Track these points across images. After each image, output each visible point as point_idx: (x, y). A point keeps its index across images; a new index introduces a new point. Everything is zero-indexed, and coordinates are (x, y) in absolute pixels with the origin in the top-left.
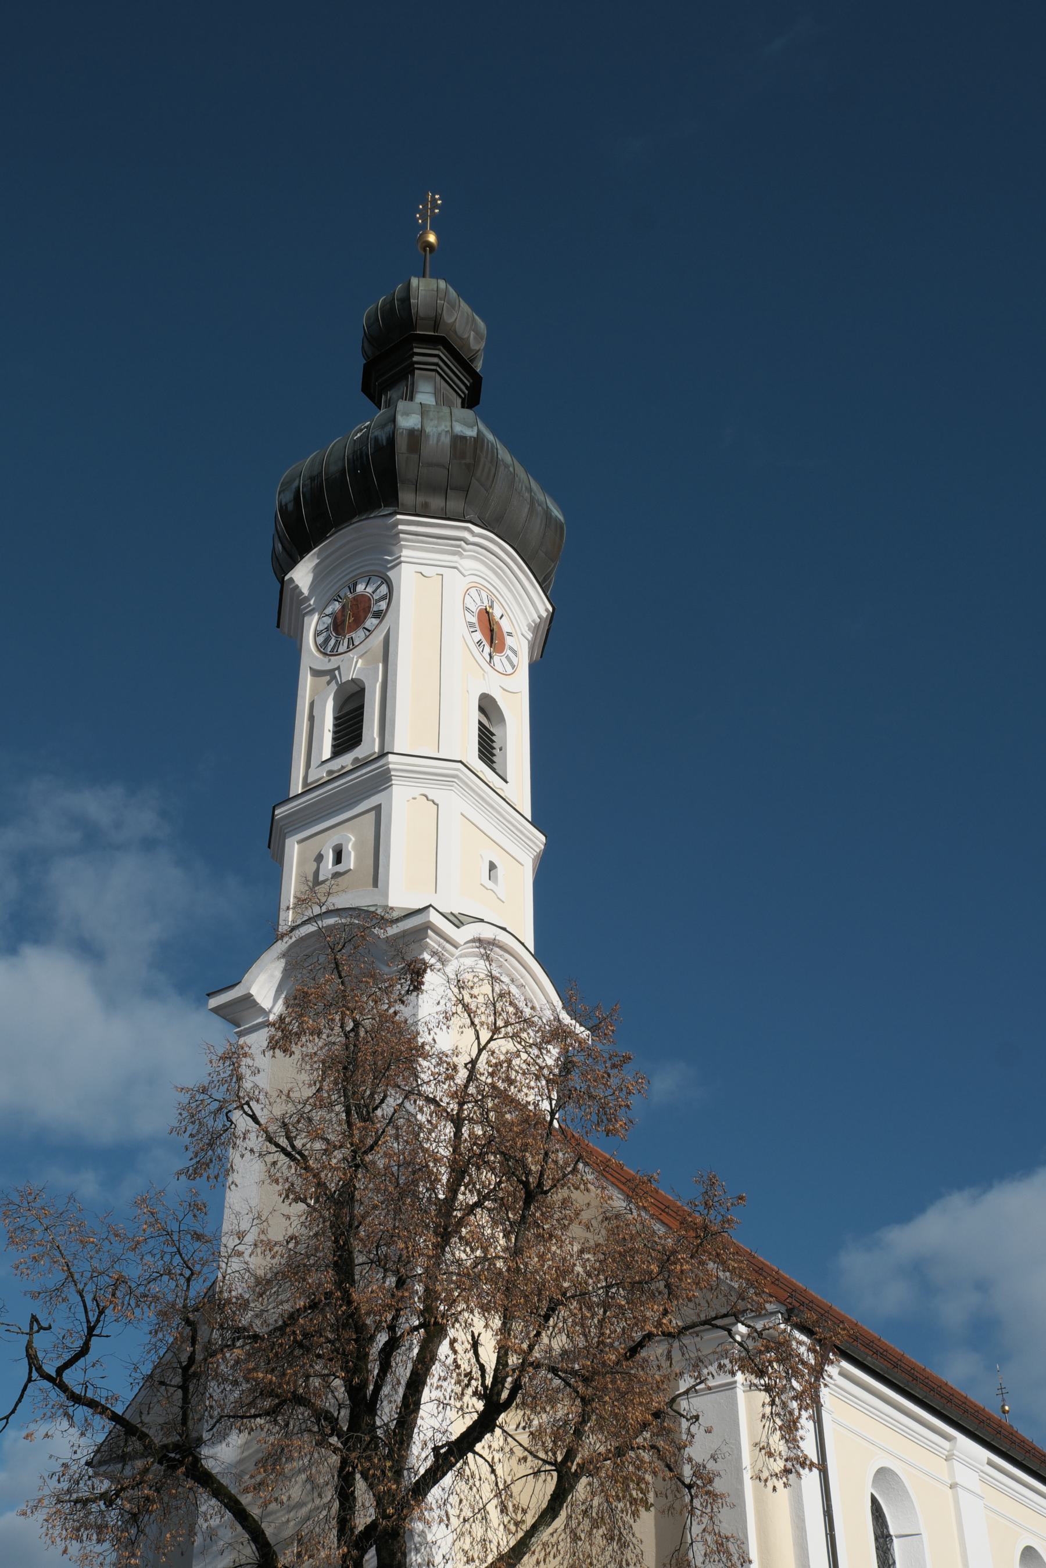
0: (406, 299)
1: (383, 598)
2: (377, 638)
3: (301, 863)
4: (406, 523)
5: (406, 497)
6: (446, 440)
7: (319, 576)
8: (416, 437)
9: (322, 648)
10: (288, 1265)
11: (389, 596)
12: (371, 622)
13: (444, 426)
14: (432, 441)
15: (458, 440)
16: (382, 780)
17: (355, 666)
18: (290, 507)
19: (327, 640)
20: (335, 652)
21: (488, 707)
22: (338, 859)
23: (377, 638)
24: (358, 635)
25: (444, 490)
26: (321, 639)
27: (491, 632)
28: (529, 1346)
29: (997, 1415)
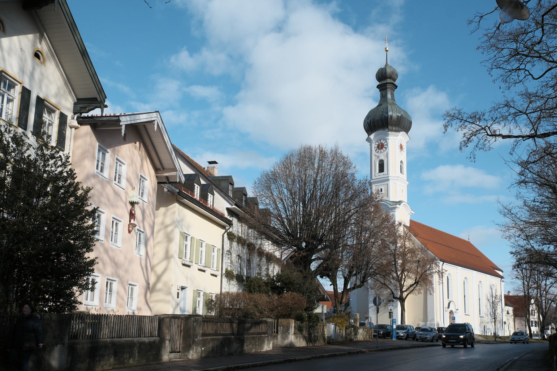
0: (386, 73)
2: (385, 153)
4: (390, 133)
5: (390, 127)
7: (375, 136)
8: (391, 116)
10: (547, 254)
11: (387, 145)
12: (384, 149)
15: (398, 117)
16: (388, 180)
17: (382, 157)
20: (378, 152)
21: (401, 162)
22: (381, 191)
24: (382, 151)
25: (395, 126)
27: (401, 147)
28: (367, 281)
29: (468, 240)
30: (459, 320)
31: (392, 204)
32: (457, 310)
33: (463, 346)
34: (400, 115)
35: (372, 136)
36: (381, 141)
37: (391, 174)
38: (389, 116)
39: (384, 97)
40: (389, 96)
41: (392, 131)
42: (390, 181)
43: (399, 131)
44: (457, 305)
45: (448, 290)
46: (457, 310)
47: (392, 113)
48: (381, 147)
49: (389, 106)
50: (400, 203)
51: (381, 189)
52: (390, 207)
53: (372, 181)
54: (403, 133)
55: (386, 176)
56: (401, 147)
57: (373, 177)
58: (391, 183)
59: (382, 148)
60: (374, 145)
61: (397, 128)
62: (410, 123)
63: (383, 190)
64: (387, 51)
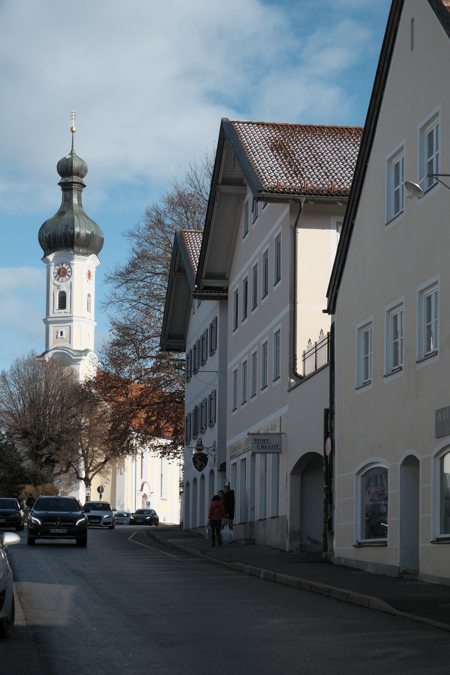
0: (72, 167)
1: (69, 272)
2: (68, 283)
3: (53, 332)
4: (76, 256)
5: (76, 249)
6: (85, 235)
7: (55, 257)
9: (55, 277)
11: (71, 272)
12: (67, 277)
13: (84, 231)
14: (82, 235)
15: (87, 235)
16: (71, 321)
17: (64, 288)
18: (48, 238)
19: (56, 276)
21: (89, 295)
22: (62, 334)
23: (68, 283)
24: (64, 279)
26: (55, 275)
27: (89, 275)
30: (151, 507)
31: (75, 354)
32: (152, 493)
33: (74, 541)
34: (90, 233)
35: (51, 257)
36: (62, 264)
37: (75, 313)
38: (76, 233)
39: (67, 200)
40: (75, 200)
41: (78, 253)
42: (74, 323)
43: (87, 254)
44: (152, 488)
45: (142, 467)
46: (152, 493)
47: (81, 230)
48: (62, 273)
49: (76, 218)
50: (86, 351)
51: (62, 333)
52: (73, 358)
53: (49, 320)
54: (93, 256)
55: (68, 315)
56: (89, 275)
57: (51, 314)
58: (75, 325)
59: (64, 276)
60: (53, 270)
61: (85, 251)
62: (102, 241)
63: (64, 333)
64: (73, 132)
